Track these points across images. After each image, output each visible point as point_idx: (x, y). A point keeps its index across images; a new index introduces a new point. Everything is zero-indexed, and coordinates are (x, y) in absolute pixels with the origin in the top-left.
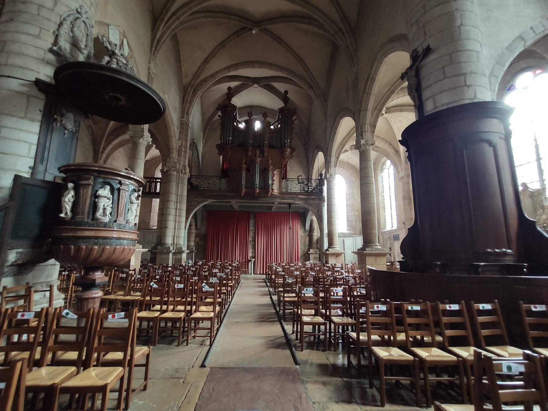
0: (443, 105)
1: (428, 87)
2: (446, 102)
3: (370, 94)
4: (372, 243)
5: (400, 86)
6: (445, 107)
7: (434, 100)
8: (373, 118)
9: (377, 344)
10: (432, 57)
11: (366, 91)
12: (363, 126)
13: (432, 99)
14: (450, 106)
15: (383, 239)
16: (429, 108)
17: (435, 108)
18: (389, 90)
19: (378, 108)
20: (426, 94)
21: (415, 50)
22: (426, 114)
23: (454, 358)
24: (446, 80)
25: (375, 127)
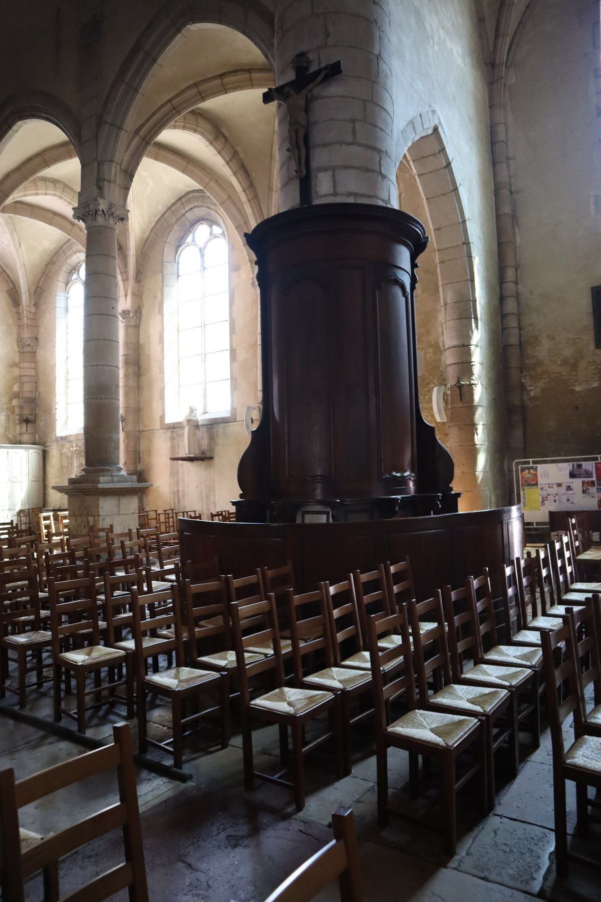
0: (349, 194)
1: (325, 145)
2: (354, 189)
3: (136, 90)
4: (109, 464)
5: (190, 105)
6: (351, 200)
7: (333, 176)
8: (128, 153)
9: (271, 678)
10: (335, 89)
11: (127, 79)
12: (106, 165)
13: (330, 173)
14: (360, 201)
15: (61, 455)
16: (324, 190)
17: (335, 194)
18: (169, 101)
19: (142, 133)
20: (320, 157)
21: (302, 55)
22: (317, 202)
23: (215, 675)
24: (355, 146)
25: (131, 176)
